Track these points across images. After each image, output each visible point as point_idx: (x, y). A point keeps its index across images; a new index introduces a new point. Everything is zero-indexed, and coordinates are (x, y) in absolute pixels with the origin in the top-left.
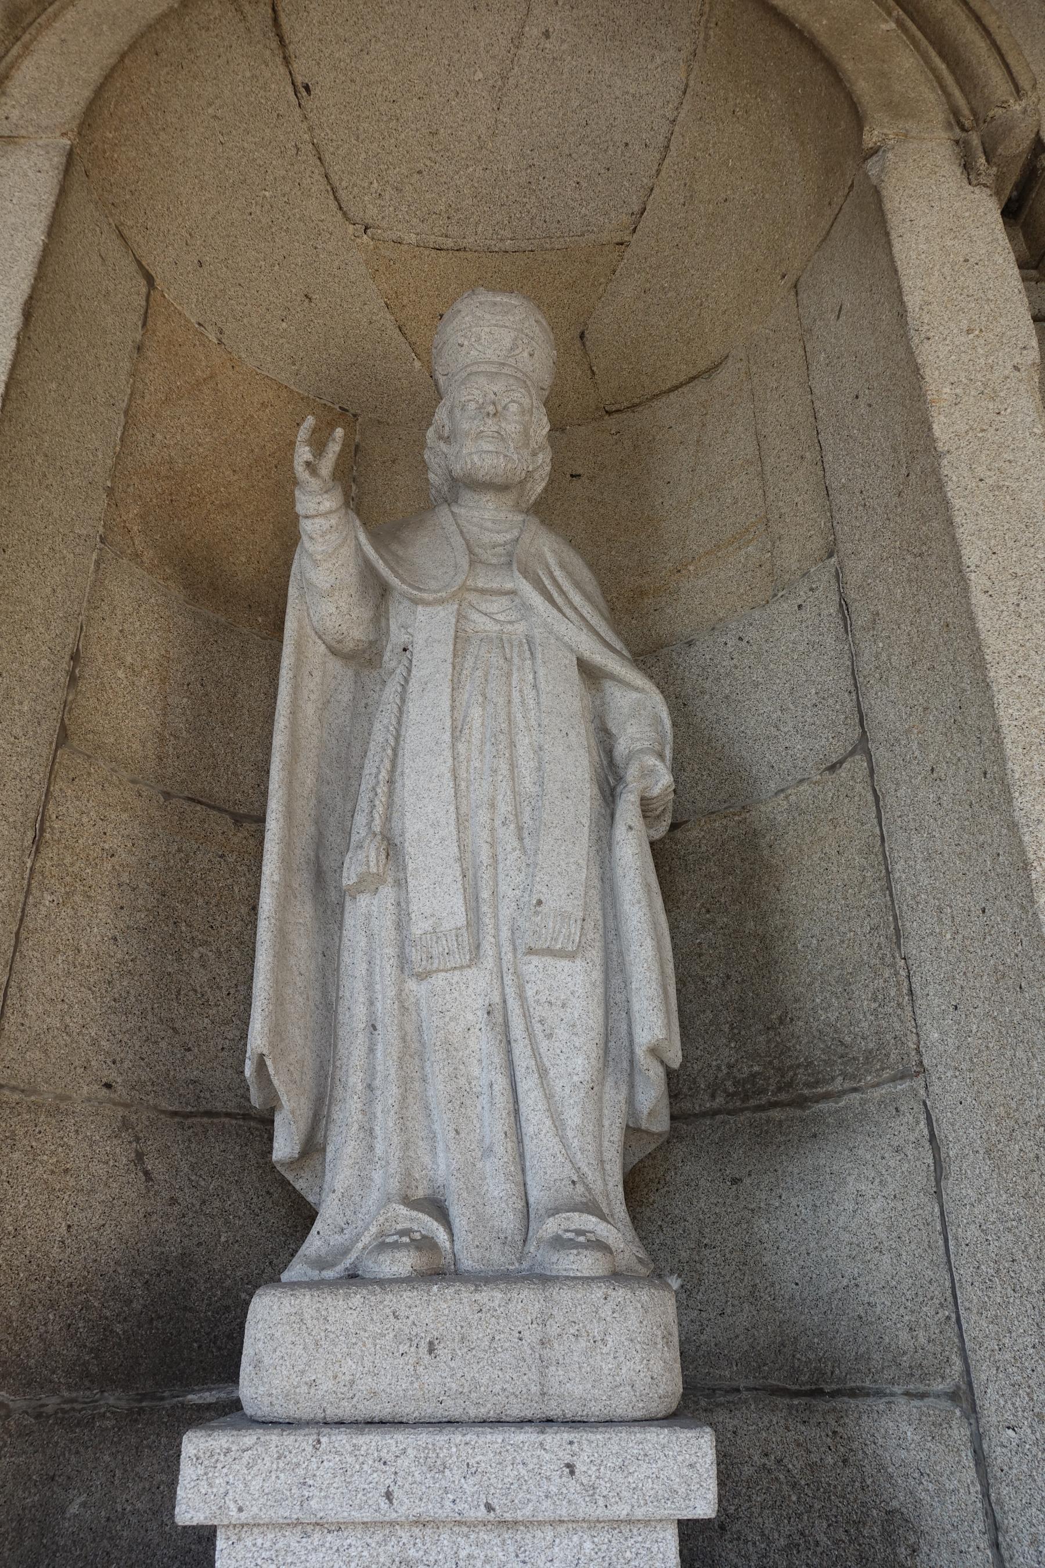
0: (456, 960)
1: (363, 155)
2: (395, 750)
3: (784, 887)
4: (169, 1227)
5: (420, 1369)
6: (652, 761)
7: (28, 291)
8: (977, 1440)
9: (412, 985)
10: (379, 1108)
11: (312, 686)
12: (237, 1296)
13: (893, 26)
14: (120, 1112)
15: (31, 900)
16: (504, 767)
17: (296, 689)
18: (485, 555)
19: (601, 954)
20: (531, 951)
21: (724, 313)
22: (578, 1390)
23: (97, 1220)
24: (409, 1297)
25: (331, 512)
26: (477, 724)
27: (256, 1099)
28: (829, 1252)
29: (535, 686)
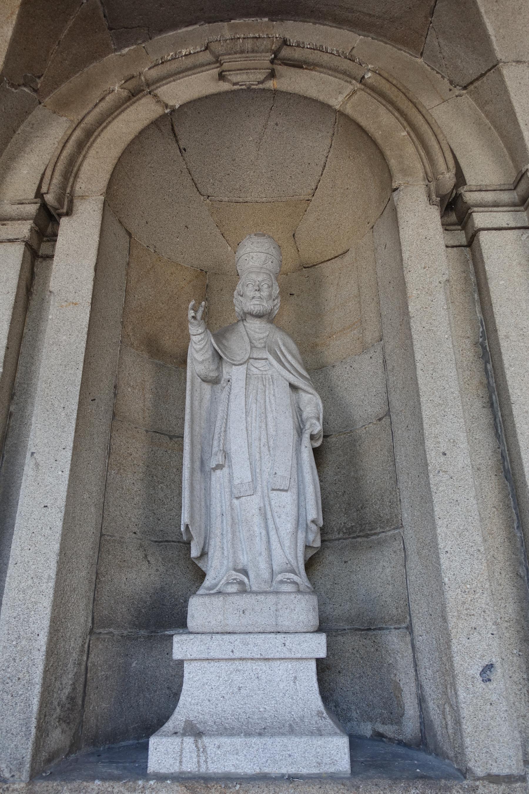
0: (249, 493)
1: (207, 170)
2: (226, 420)
3: (363, 461)
4: (156, 579)
5: (240, 618)
6: (314, 421)
7: (95, 261)
8: (412, 640)
9: (235, 501)
10: (225, 541)
11: (197, 395)
12: (179, 601)
13: (406, 133)
14: (139, 541)
15: (108, 474)
16: (264, 426)
17: (192, 397)
18: (257, 344)
19: (297, 490)
20: (273, 490)
21: (348, 232)
22: (287, 623)
23: (134, 577)
24: (237, 597)
25: (202, 333)
26: (254, 410)
27: (185, 538)
28: (374, 585)
29: (274, 395)
